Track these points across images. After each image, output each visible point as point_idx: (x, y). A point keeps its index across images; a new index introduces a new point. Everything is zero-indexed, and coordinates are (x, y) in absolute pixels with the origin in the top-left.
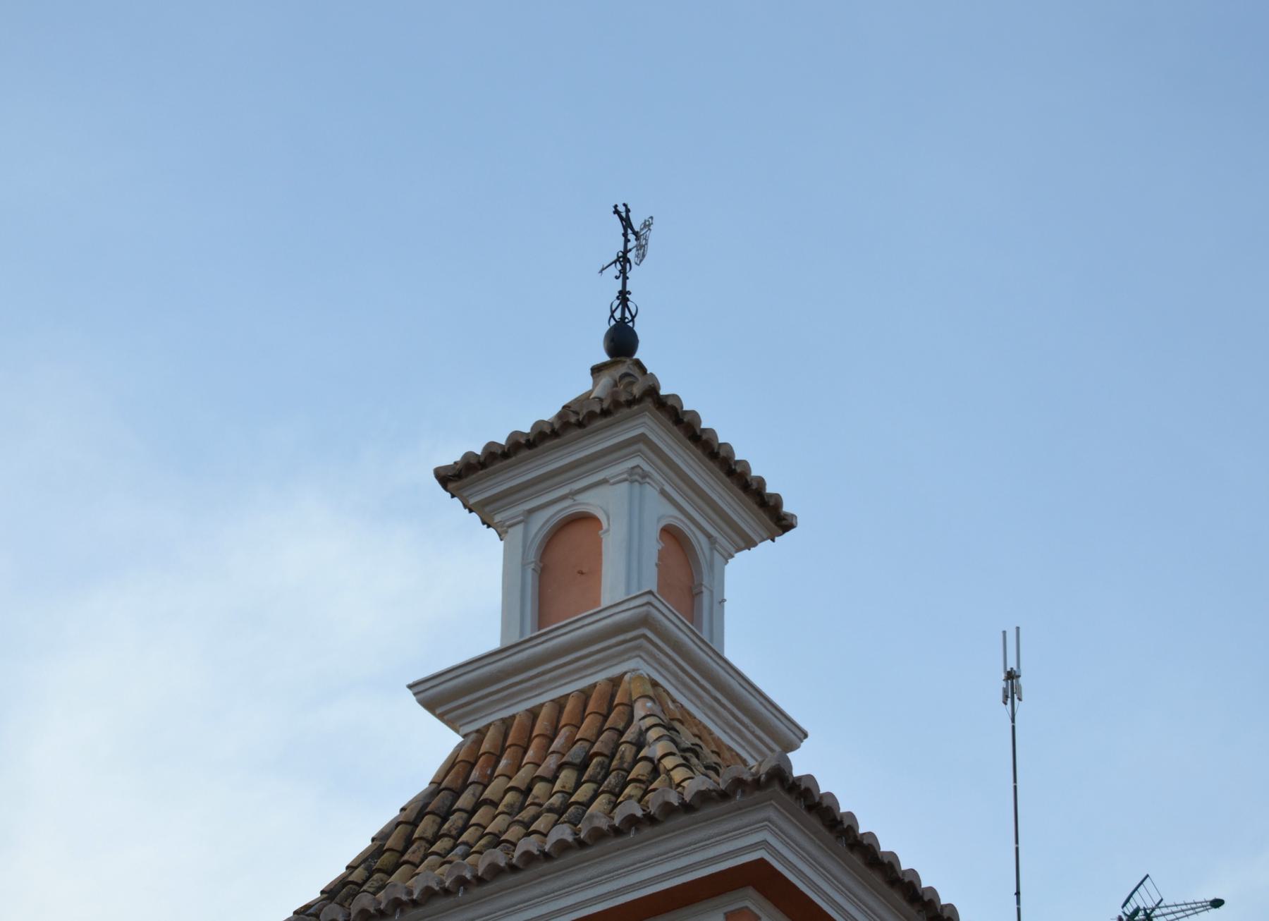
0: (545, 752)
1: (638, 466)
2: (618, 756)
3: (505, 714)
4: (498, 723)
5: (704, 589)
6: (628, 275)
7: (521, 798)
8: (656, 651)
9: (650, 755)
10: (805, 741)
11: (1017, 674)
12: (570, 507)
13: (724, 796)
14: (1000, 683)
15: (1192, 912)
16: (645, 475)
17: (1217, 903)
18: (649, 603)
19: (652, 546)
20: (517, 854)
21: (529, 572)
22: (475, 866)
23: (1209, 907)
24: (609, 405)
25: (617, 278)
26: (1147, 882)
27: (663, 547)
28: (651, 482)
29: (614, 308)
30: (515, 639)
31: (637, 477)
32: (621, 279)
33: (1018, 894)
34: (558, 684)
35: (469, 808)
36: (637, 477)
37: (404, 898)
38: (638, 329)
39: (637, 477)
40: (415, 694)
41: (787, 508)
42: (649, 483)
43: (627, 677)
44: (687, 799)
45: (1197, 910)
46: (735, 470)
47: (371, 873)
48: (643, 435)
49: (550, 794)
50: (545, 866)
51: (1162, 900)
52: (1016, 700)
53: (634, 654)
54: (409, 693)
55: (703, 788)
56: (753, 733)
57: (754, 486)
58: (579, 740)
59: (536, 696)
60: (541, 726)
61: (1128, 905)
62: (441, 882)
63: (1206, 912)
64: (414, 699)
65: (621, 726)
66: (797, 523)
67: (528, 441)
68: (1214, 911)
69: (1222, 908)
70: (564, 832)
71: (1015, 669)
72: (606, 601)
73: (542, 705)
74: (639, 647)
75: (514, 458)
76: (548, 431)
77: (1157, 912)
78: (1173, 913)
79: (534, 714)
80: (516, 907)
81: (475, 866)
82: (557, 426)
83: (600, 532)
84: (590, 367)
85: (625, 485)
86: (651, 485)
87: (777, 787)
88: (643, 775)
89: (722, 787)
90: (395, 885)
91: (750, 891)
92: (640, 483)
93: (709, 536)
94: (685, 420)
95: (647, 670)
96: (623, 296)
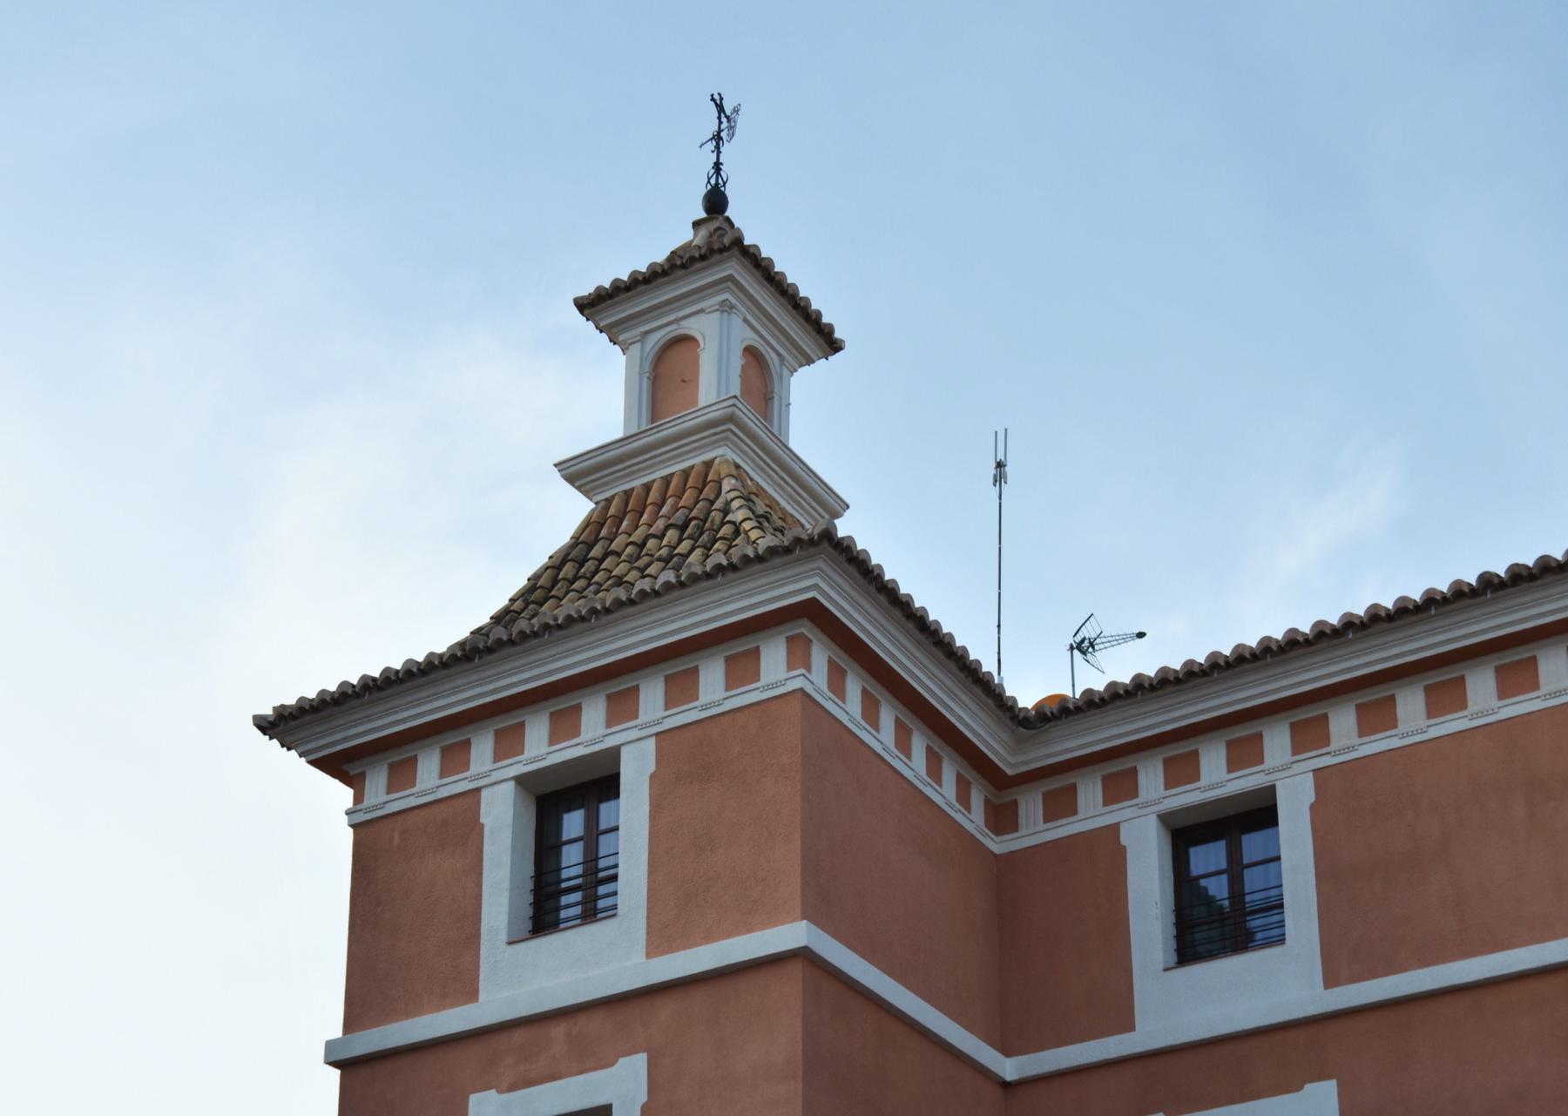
1: (727, 300)
2: (709, 520)
5: (775, 395)
9: (734, 520)
10: (847, 511)
12: (676, 329)
16: (732, 307)
17: (1141, 635)
18: (734, 405)
21: (645, 379)
30: (634, 430)
31: (726, 308)
33: (999, 626)
37: (552, 623)
39: (726, 308)
41: (838, 335)
48: (731, 276)
54: (556, 470)
55: (772, 544)
56: (809, 505)
57: (814, 317)
62: (579, 612)
63: (1132, 642)
64: (559, 474)
68: (1138, 640)
69: (1145, 638)
71: (1003, 460)
72: (702, 402)
73: (654, 481)
79: (648, 487)
85: (717, 314)
87: (826, 545)
91: (805, 622)
92: (729, 313)
93: (779, 355)
95: (732, 456)
96: (717, 167)
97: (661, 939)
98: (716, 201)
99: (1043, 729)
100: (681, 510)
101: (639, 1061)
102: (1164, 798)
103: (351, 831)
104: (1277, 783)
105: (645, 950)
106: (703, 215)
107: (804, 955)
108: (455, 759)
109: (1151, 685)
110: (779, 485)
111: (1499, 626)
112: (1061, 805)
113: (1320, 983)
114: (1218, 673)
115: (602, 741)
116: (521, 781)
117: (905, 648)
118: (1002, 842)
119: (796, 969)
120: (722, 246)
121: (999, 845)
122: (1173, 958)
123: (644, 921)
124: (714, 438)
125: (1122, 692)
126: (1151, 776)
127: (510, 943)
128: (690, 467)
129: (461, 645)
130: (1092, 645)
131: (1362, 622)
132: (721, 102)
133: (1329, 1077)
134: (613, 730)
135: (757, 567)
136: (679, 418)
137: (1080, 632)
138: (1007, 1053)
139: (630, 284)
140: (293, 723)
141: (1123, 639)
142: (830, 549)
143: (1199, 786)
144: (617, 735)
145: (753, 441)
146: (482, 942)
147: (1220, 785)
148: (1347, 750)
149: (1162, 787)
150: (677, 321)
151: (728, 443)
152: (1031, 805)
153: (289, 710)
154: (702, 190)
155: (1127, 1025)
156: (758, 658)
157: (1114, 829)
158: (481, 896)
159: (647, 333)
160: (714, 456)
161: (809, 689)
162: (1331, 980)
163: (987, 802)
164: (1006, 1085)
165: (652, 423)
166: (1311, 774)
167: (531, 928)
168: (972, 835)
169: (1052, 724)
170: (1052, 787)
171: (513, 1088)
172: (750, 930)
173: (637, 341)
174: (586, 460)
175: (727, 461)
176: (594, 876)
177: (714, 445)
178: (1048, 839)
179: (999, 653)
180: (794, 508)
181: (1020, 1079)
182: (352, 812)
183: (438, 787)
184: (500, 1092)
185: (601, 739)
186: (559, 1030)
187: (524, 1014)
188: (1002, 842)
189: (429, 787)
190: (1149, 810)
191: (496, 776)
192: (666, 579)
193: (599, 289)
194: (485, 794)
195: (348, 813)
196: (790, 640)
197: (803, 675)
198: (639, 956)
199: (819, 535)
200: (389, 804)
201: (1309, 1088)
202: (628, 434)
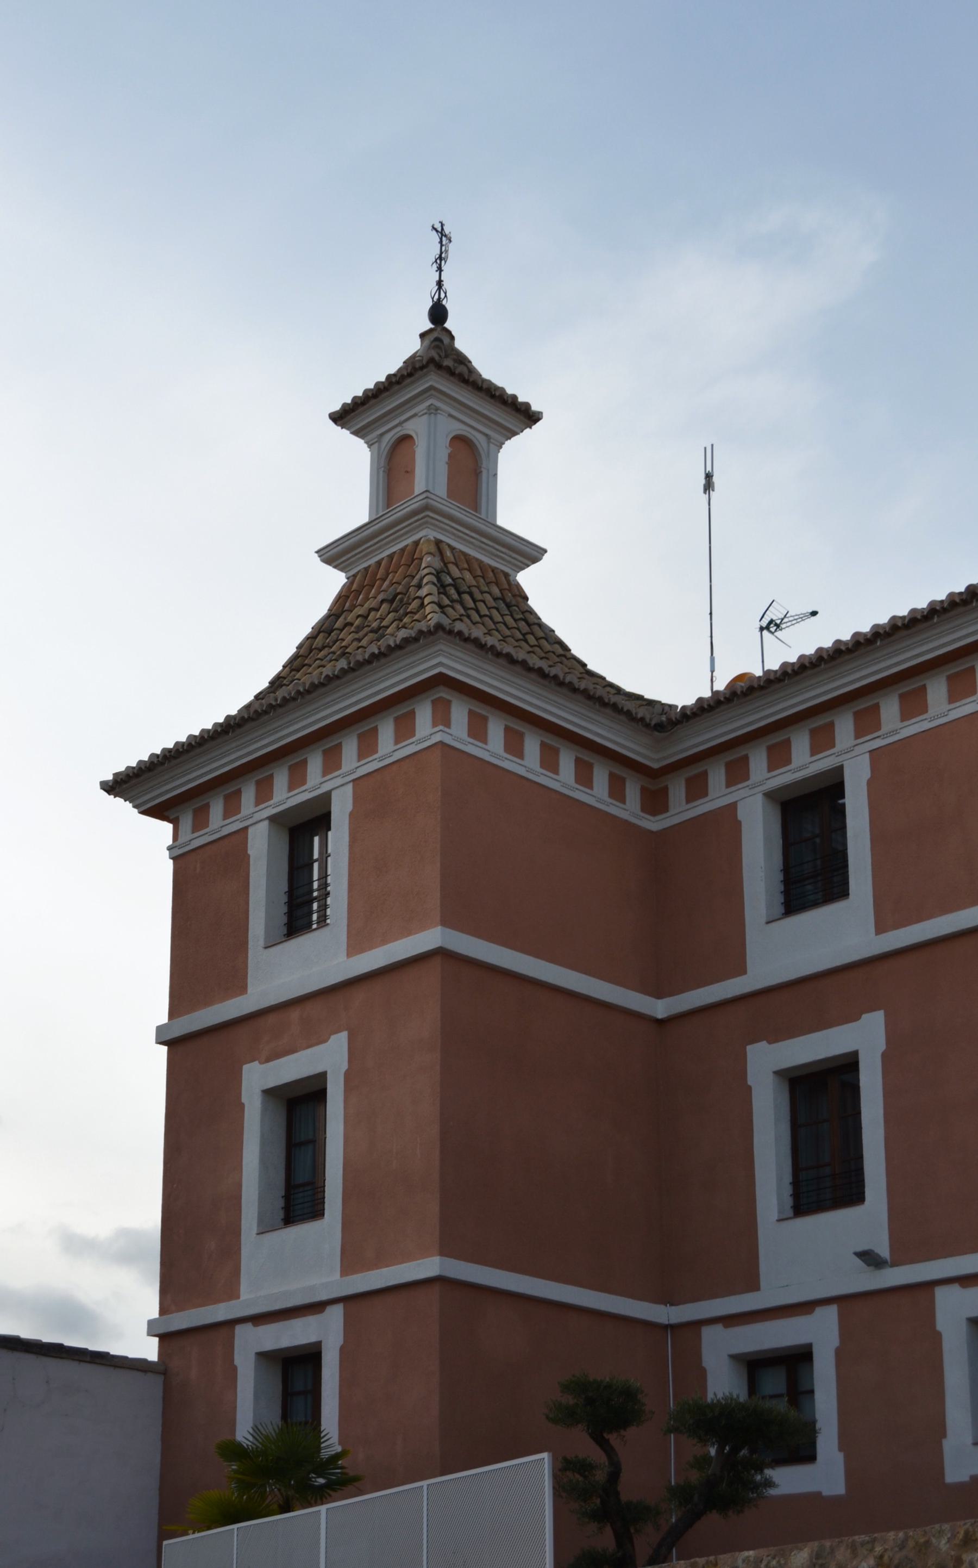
0: (379, 593)
1: (432, 404)
2: (408, 594)
3: (365, 565)
4: (362, 570)
5: (483, 469)
6: (443, 269)
7: (389, 606)
8: (437, 523)
9: (420, 595)
10: (546, 555)
11: (711, 475)
12: (400, 431)
13: (416, 639)
14: (702, 481)
15: (800, 620)
16: (437, 409)
17: (814, 613)
18: (427, 497)
19: (443, 453)
20: (323, 677)
21: (381, 473)
22: (304, 683)
23: (810, 616)
24: (411, 369)
25: (437, 271)
26: (774, 602)
27: (451, 451)
28: (441, 412)
29: (432, 296)
30: (374, 517)
31: (432, 411)
32: (438, 272)
33: (711, 614)
34: (389, 546)
35: (341, 628)
36: (433, 411)
37: (274, 703)
38: (448, 306)
39: (432, 411)
40: (320, 556)
41: (535, 407)
42: (439, 414)
43: (422, 541)
44: (398, 642)
45: (803, 618)
46: (495, 394)
47: (291, 671)
48: (431, 386)
49: (389, 611)
50: (338, 682)
51: (788, 612)
52: (711, 492)
53: (424, 526)
54: (316, 555)
55: (405, 636)
56: (510, 556)
57: (510, 401)
58: (395, 583)
59: (380, 553)
60: (382, 571)
61: (763, 619)
62: (290, 694)
63: (809, 619)
64: (319, 559)
65: (414, 574)
66: (542, 416)
67: (373, 394)
68: (813, 618)
69: (818, 615)
70: (342, 664)
71: (710, 471)
72: (417, 492)
73: (383, 559)
74: (427, 522)
75: (367, 405)
76: (382, 388)
77: (786, 620)
78: (790, 621)
79: (379, 563)
80: (415, 664)
81: (304, 683)
82: (386, 385)
83: (415, 447)
84: (419, 334)
85: (426, 417)
86: (442, 414)
87: (441, 633)
88: (415, 609)
89: (413, 635)
90: (350, 654)
91: (441, 688)
92: (435, 414)
93: (486, 435)
94: (457, 372)
95: (432, 534)
96: (440, 283)
97: (357, 944)
98: (438, 313)
99: (672, 731)
100: (395, 585)
101: (343, 1036)
102: (766, 779)
103: (171, 861)
104: (844, 763)
105: (346, 951)
106: (429, 326)
107: (441, 953)
108: (232, 807)
109: (811, 663)
110: (480, 548)
111: (828, 691)
112: (697, 789)
113: (873, 930)
114: (881, 640)
115: (319, 788)
116: (274, 820)
117: (533, 692)
118: (657, 821)
119: (437, 962)
120: (421, 365)
121: (654, 824)
122: (781, 910)
123: (345, 928)
124: (418, 523)
125: (722, 699)
126: (758, 761)
127: (266, 948)
128: (405, 546)
129: (247, 707)
130: (778, 626)
131: (709, 705)
132: (442, 229)
133: (879, 1009)
134: (399, 746)
135: (399, 653)
136: (393, 509)
137: (765, 616)
138: (659, 995)
139: (353, 406)
140: (124, 786)
141: (802, 618)
142: (445, 636)
143: (789, 769)
144: (329, 782)
145: (450, 520)
146: (249, 947)
147: (895, 732)
148: (885, 736)
149: (766, 770)
150: (400, 424)
151: (429, 526)
152: (677, 790)
153: (121, 777)
154: (430, 304)
155: (741, 970)
156: (414, 718)
157: (733, 807)
158: (248, 911)
159: (382, 435)
160: (421, 536)
161: (448, 740)
162: (881, 928)
163: (644, 790)
164: (660, 1022)
165: (388, 509)
166: (868, 754)
167: (286, 932)
168: (626, 821)
169: (678, 726)
170: (952, 671)
171: (268, 1060)
172: (409, 934)
173: (376, 442)
174: (399, 511)
175: (428, 541)
176: (324, 890)
177: (419, 528)
178: (688, 817)
179: (711, 637)
180: (497, 562)
181: (668, 1017)
182: (172, 848)
183: (222, 827)
184: (261, 1063)
185: (319, 786)
186: (295, 1014)
187: (273, 1003)
188: (657, 821)
189: (216, 827)
190: (757, 790)
191: (257, 817)
192: (341, 667)
193: (344, 405)
194: (250, 830)
195: (170, 848)
196: (434, 703)
197: (441, 730)
198: (342, 957)
199: (434, 627)
200: (193, 841)
201: (865, 1017)
202: (373, 519)
